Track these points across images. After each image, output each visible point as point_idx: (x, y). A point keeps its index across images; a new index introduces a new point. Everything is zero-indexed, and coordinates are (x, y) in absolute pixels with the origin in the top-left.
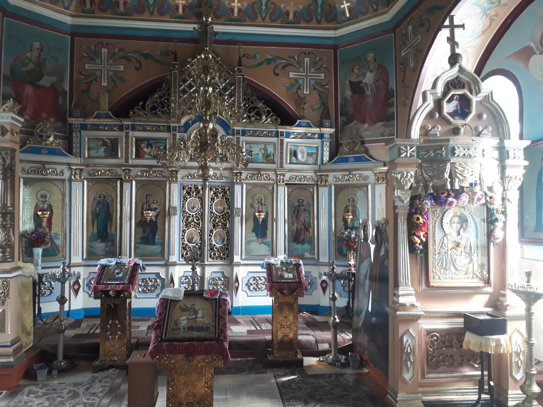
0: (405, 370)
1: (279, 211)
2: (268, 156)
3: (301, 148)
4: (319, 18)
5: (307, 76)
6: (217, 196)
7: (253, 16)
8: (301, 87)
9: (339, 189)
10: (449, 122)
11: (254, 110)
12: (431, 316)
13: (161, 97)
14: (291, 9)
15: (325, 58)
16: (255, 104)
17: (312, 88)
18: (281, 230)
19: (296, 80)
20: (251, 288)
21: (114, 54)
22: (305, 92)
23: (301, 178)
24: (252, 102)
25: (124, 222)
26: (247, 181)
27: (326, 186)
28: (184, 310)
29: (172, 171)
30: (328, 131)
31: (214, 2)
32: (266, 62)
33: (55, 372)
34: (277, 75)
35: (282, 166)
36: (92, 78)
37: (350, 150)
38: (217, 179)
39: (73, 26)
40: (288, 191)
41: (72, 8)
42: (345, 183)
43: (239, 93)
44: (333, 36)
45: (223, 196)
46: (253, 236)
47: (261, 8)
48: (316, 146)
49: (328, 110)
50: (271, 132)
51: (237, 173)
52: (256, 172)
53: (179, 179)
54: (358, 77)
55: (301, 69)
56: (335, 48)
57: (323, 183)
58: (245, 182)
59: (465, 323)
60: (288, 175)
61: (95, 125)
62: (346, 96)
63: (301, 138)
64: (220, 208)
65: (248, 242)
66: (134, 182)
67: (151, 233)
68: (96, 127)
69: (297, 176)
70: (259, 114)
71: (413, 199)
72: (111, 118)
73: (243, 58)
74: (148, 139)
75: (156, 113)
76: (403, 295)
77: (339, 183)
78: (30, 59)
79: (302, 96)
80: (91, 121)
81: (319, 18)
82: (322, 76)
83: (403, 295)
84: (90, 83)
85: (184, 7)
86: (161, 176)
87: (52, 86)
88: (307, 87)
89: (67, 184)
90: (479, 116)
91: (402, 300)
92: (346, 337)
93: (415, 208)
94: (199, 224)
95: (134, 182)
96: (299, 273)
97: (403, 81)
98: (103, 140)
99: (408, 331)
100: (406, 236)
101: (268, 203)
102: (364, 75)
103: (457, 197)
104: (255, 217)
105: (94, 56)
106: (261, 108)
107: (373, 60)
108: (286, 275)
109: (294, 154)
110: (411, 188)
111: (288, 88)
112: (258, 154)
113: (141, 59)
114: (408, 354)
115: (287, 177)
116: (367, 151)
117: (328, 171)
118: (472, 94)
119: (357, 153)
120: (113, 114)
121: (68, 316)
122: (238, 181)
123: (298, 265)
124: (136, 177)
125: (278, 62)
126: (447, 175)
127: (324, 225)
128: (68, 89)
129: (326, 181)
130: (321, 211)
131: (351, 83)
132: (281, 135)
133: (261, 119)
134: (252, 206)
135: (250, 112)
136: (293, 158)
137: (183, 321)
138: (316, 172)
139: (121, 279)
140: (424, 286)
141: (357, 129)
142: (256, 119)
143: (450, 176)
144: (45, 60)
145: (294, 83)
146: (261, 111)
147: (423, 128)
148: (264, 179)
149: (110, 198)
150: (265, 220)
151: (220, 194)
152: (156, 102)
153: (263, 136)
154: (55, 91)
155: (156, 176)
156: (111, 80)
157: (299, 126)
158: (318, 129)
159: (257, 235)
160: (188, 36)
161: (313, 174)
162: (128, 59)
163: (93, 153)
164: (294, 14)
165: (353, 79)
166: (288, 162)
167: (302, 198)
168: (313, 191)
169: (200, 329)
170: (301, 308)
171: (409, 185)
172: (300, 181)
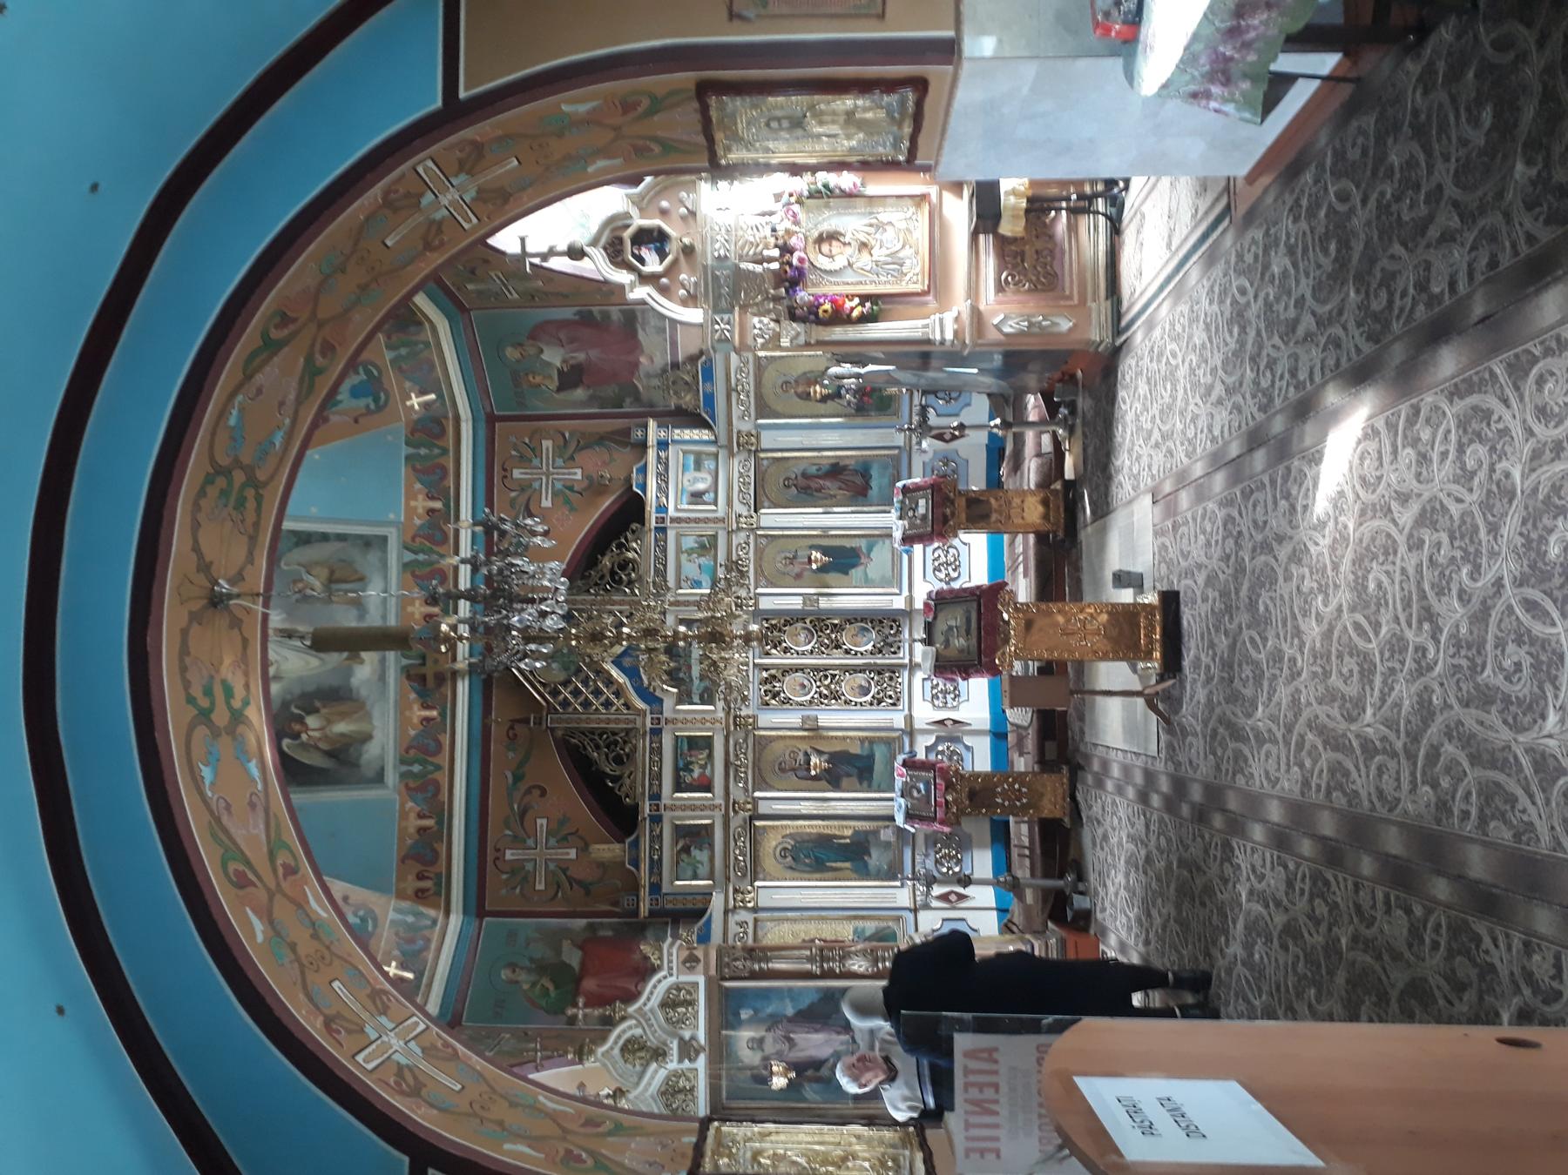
0: (1055, 329)
1: (807, 524)
2: (703, 546)
3: (686, 483)
4: (436, 451)
9: (763, 409)
10: (675, 262)
12: (973, 290)
13: (598, 747)
14: (421, 504)
18: (844, 520)
20: (954, 575)
21: (515, 837)
22: (579, 477)
24: (602, 577)
25: (831, 812)
28: (947, 643)
29: (735, 724)
30: (653, 432)
31: (1550, 305)
33: (1081, 887)
35: (723, 520)
36: (562, 876)
39: (465, 912)
41: (432, 913)
46: (856, 573)
47: (422, 563)
49: (614, 433)
53: (750, 713)
55: (536, 485)
56: (492, 420)
59: (986, 232)
61: (651, 868)
64: (802, 638)
65: (868, 583)
66: (757, 794)
67: (851, 766)
68: (656, 866)
70: (624, 565)
71: (793, 317)
72: (637, 838)
74: (677, 770)
76: (942, 332)
78: (534, 984)
79: (586, 482)
80: (644, 877)
83: (942, 332)
84: (569, 879)
85: (426, 707)
87: (581, 948)
89: (761, 915)
90: (664, 213)
91: (949, 336)
92: (1033, 405)
93: (809, 315)
94: (834, 676)
95: (757, 794)
96: (918, 488)
97: (566, 296)
98: (679, 852)
99: (997, 327)
100: (850, 328)
101: (792, 545)
102: (548, 364)
103: (791, 251)
104: (819, 570)
105: (519, 873)
108: (921, 510)
109: (697, 497)
110: (777, 321)
113: (523, 786)
114: (1031, 325)
115: (744, 511)
116: (693, 359)
117: (730, 431)
118: (628, 226)
119: (695, 377)
120: (630, 834)
121: (1006, 911)
123: (905, 490)
124: (746, 790)
126: (758, 268)
127: (834, 438)
128: (582, 922)
129: (749, 435)
130: (807, 444)
131: (560, 389)
133: (633, 561)
134: (798, 576)
135: (620, 581)
136: (706, 498)
137: (959, 642)
138: (731, 454)
139: (927, 784)
140: (930, 298)
141: (648, 376)
143: (760, 262)
144: (531, 960)
146: (616, 559)
147: (684, 303)
150: (825, 551)
154: (587, 943)
156: (564, 841)
157: (644, 487)
159: (854, 566)
160: (478, 698)
162: (523, 813)
163: (703, 870)
164: (432, 498)
169: (968, 621)
170: (994, 482)
171: (772, 324)
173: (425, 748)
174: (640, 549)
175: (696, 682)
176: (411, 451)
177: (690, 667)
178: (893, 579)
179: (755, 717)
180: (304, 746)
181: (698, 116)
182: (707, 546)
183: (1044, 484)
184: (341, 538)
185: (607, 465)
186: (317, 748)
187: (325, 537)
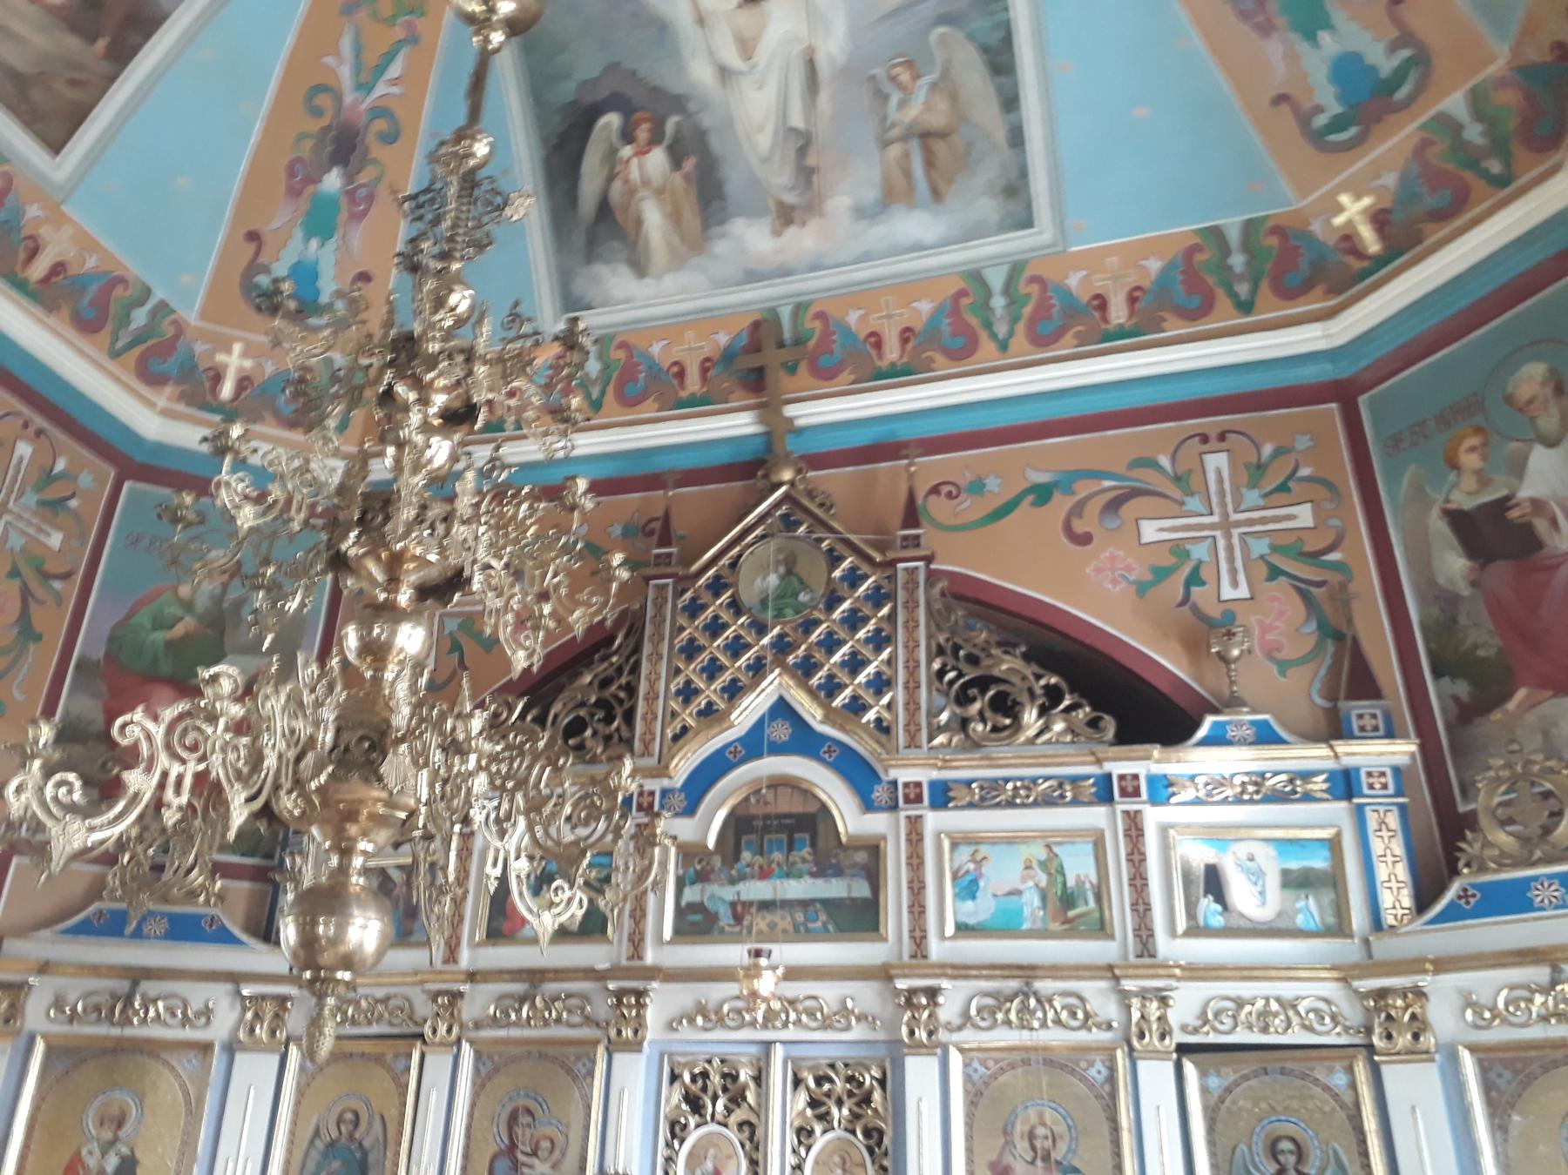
4: (1243, 289)
5: (1226, 526)
6: (824, 1117)
7: (959, 342)
8: (1205, 573)
11: (983, 692)
15: (1303, 443)
16: (986, 662)
17: (1264, 571)
19: (1178, 550)
22: (1227, 592)
23: (1265, 1014)
24: (973, 660)
26: (969, 1037)
27: (1425, 1055)
30: (1383, 755)
32: (1030, 498)
34: (1084, 539)
37: (1524, 840)
38: (826, 1025)
40: (1204, 1090)
42: (1536, 1032)
43: (911, 625)
44: (1322, 345)
45: (855, 1116)
47: (986, 305)
48: (1326, 834)
50: (1075, 780)
51: (912, 992)
52: (1014, 984)
54: (1483, 480)
55: (1194, 503)
56: (1344, 393)
57: (1403, 1040)
58: (956, 1037)
60: (1186, 1002)
62: (1441, 581)
63: (1238, 800)
66: (467, 1050)
69: (1240, 1003)
70: (1006, 706)
73: (933, 498)
75: (580, 747)
77: (1499, 1034)
78: (188, 606)
79: (1214, 612)
81: (1243, 289)
82: (1304, 516)
86: (576, 1019)
88: (1233, 572)
95: (467, 1050)
102: (1518, 468)
106: (1015, 680)
107: (1549, 391)
111: (1142, 589)
112: (1017, 893)
117: (1415, 965)
122: (921, 1034)
124: (478, 1025)
125: (1083, 489)
129: (1419, 1026)
131: (1459, 520)
132: (1124, 793)
133: (1017, 726)
135: (963, 699)
136: (1207, 905)
138: (1346, 973)
142: (995, 729)
145: (1169, 561)
146: (1018, 691)
148: (1058, 1022)
149: (377, 1127)
151: (840, 1103)
152: (582, 704)
153: (1035, 804)
155: (558, 1020)
157: (1217, 740)
158: (1322, 751)
160: (721, 457)
161: (1330, 989)
164: (1132, 300)
165: (1464, 501)
166: (1182, 924)
167: (1290, 1129)
168: (1353, 1085)
172: (1265, 1030)
173: (640, 382)
174: (1047, 743)
175: (728, 893)
176: (1234, 236)
177: (764, 874)
179: (635, 1046)
180: (612, 152)
184: (1017, 138)
185: (1272, 637)
186: (611, 179)
187: (1010, 102)
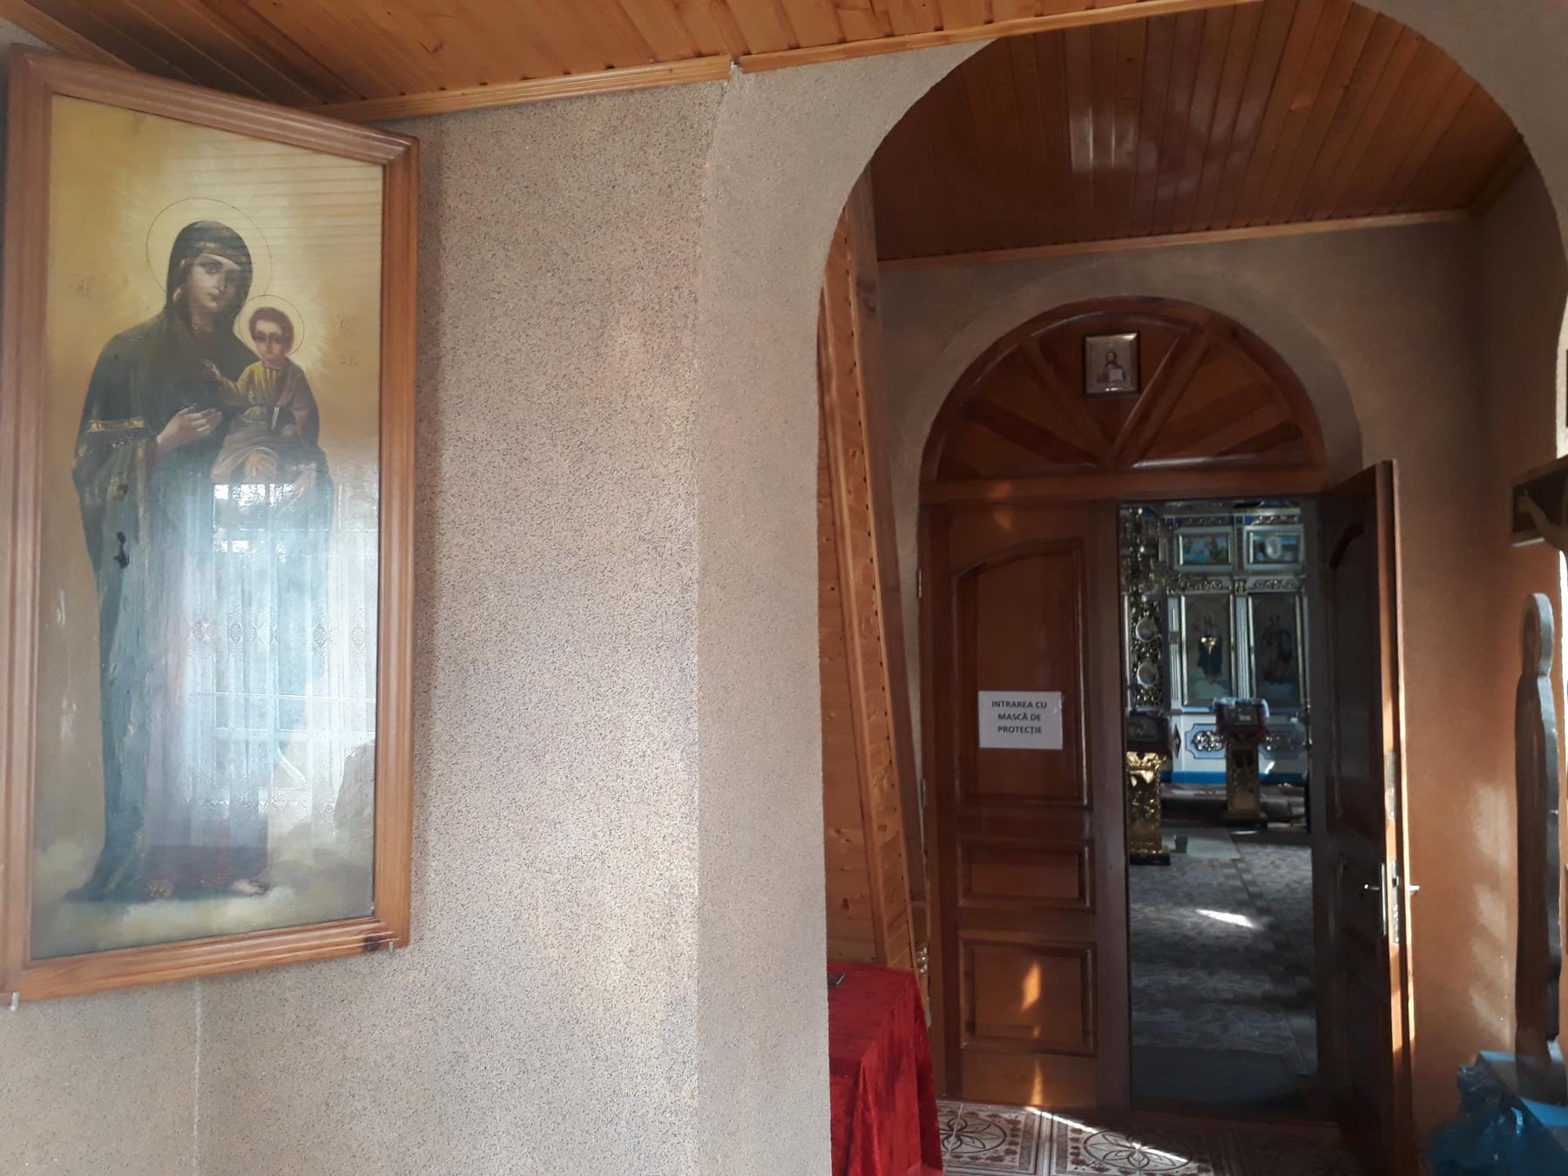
18: (1244, 662)
46: (1200, 672)
64: (1145, 631)
109: (1260, 547)
136: (1261, 557)
150: (1217, 648)
159: (1206, 672)
178: (1194, 700)
181: (334, 965)
182: (1218, 557)
183: (1265, 807)
